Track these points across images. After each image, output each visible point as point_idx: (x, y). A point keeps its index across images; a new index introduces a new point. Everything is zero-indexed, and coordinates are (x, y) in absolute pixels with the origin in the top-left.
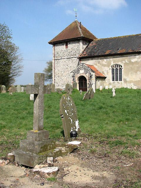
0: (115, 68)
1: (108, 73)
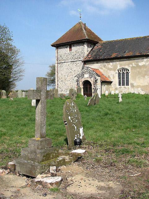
0: (121, 72)
1: (114, 77)
